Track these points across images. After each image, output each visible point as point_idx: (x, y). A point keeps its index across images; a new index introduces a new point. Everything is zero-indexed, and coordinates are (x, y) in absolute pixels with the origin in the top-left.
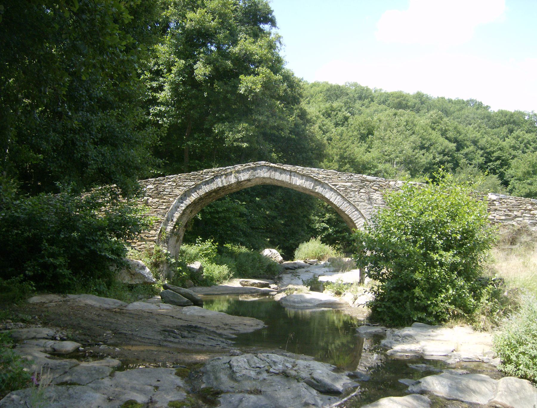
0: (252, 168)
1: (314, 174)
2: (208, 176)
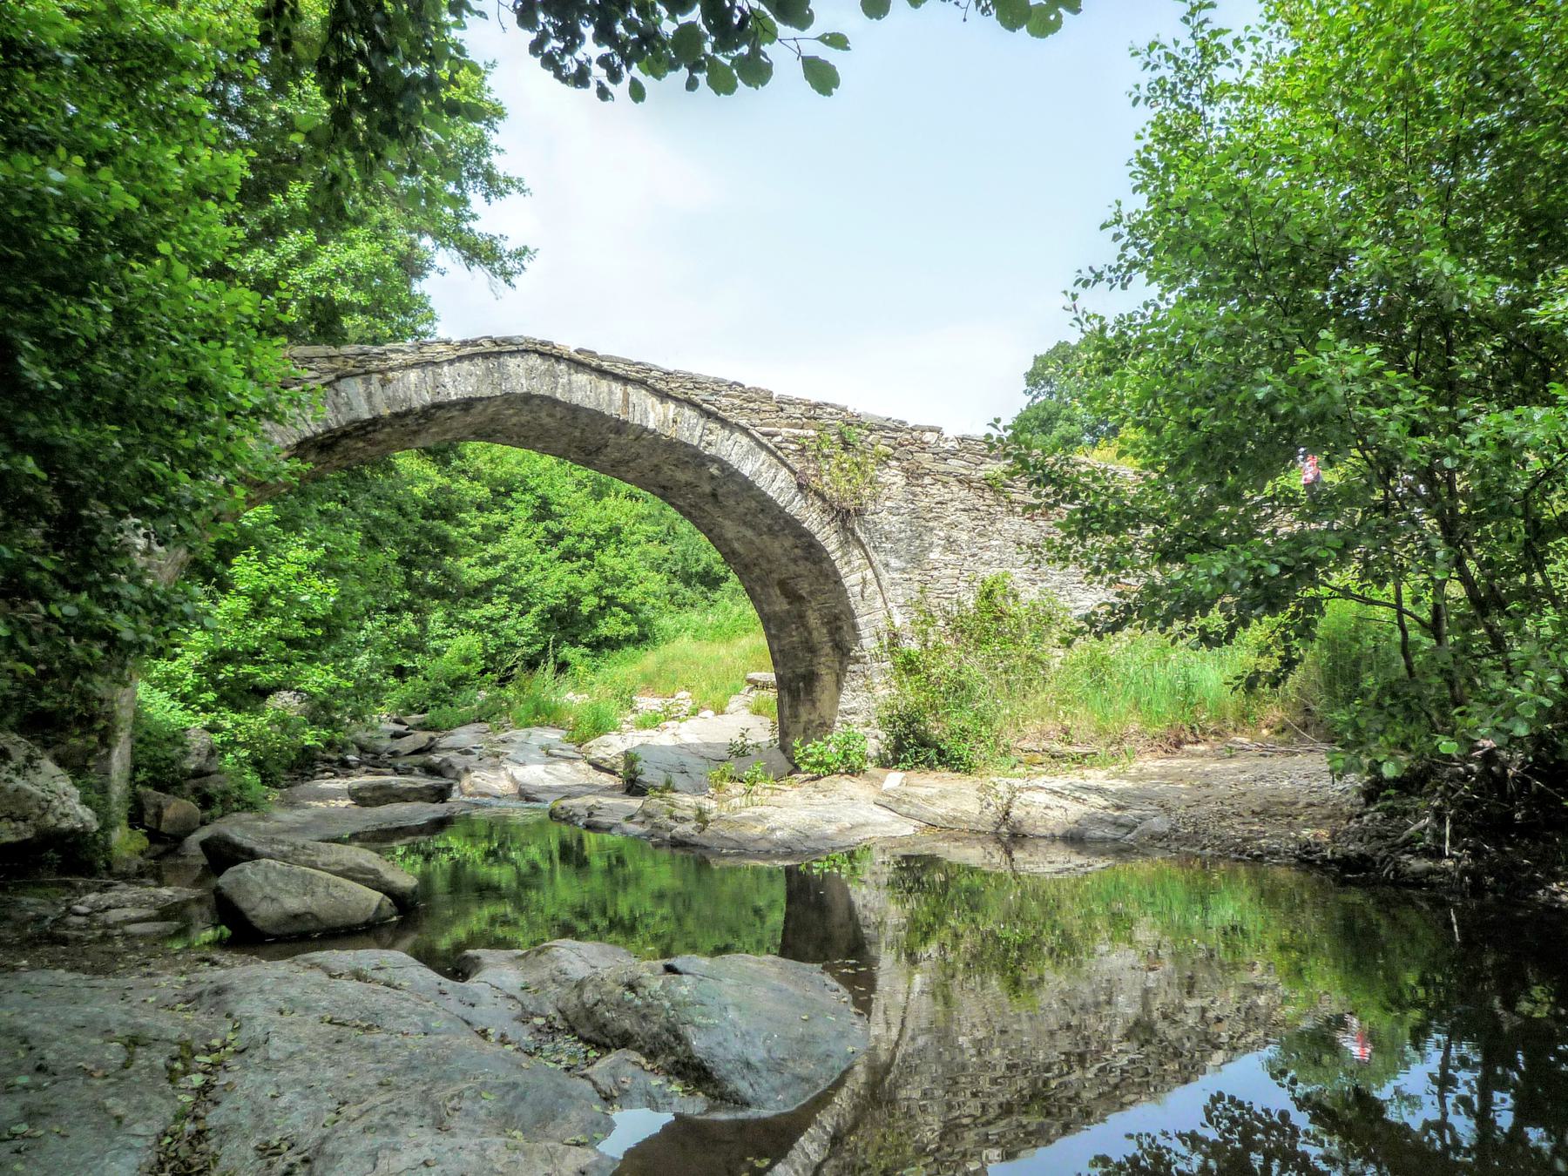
1: (704, 395)
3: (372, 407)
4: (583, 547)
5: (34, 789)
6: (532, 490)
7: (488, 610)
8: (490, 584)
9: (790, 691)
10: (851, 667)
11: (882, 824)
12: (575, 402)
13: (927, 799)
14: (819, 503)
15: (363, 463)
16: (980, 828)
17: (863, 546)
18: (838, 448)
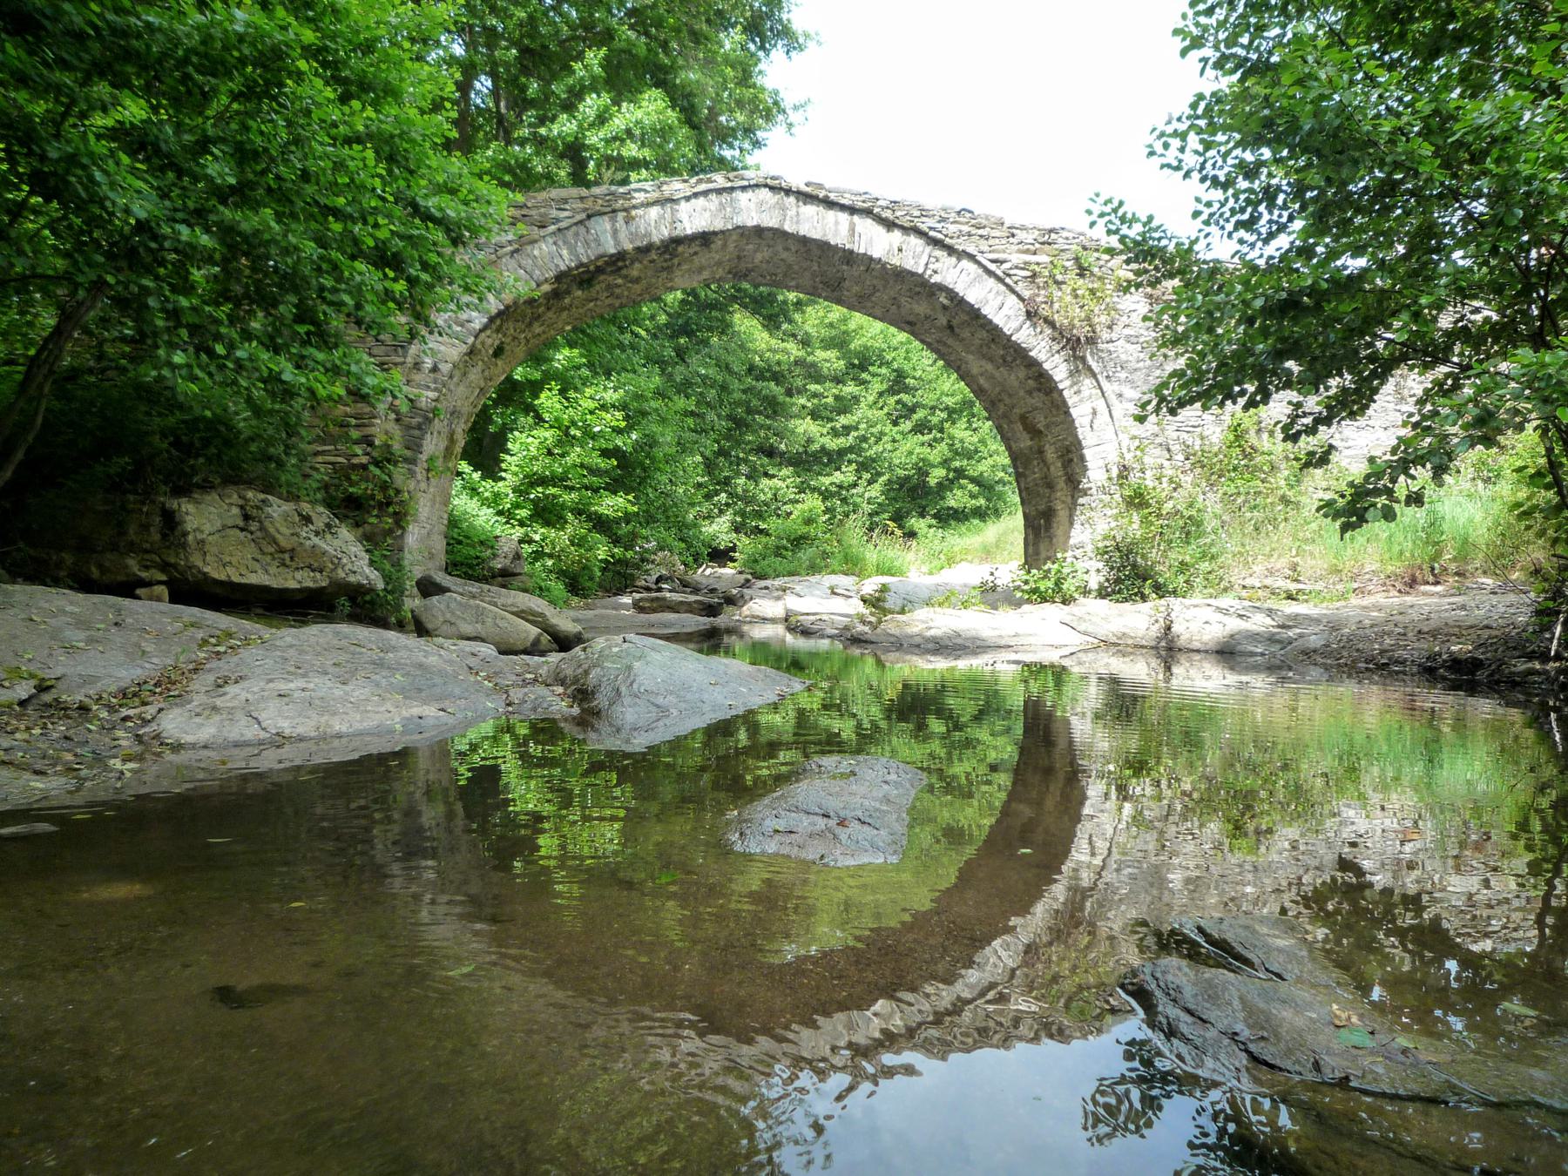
0: (719, 191)
1: (931, 222)
2: (566, 214)
3: (617, 242)
4: (935, 420)
5: (327, 548)
6: (888, 364)
7: (838, 477)
8: (842, 452)
10: (1081, 501)
12: (802, 233)
14: (1048, 331)
15: (710, 329)
17: (1094, 375)
18: (1072, 275)
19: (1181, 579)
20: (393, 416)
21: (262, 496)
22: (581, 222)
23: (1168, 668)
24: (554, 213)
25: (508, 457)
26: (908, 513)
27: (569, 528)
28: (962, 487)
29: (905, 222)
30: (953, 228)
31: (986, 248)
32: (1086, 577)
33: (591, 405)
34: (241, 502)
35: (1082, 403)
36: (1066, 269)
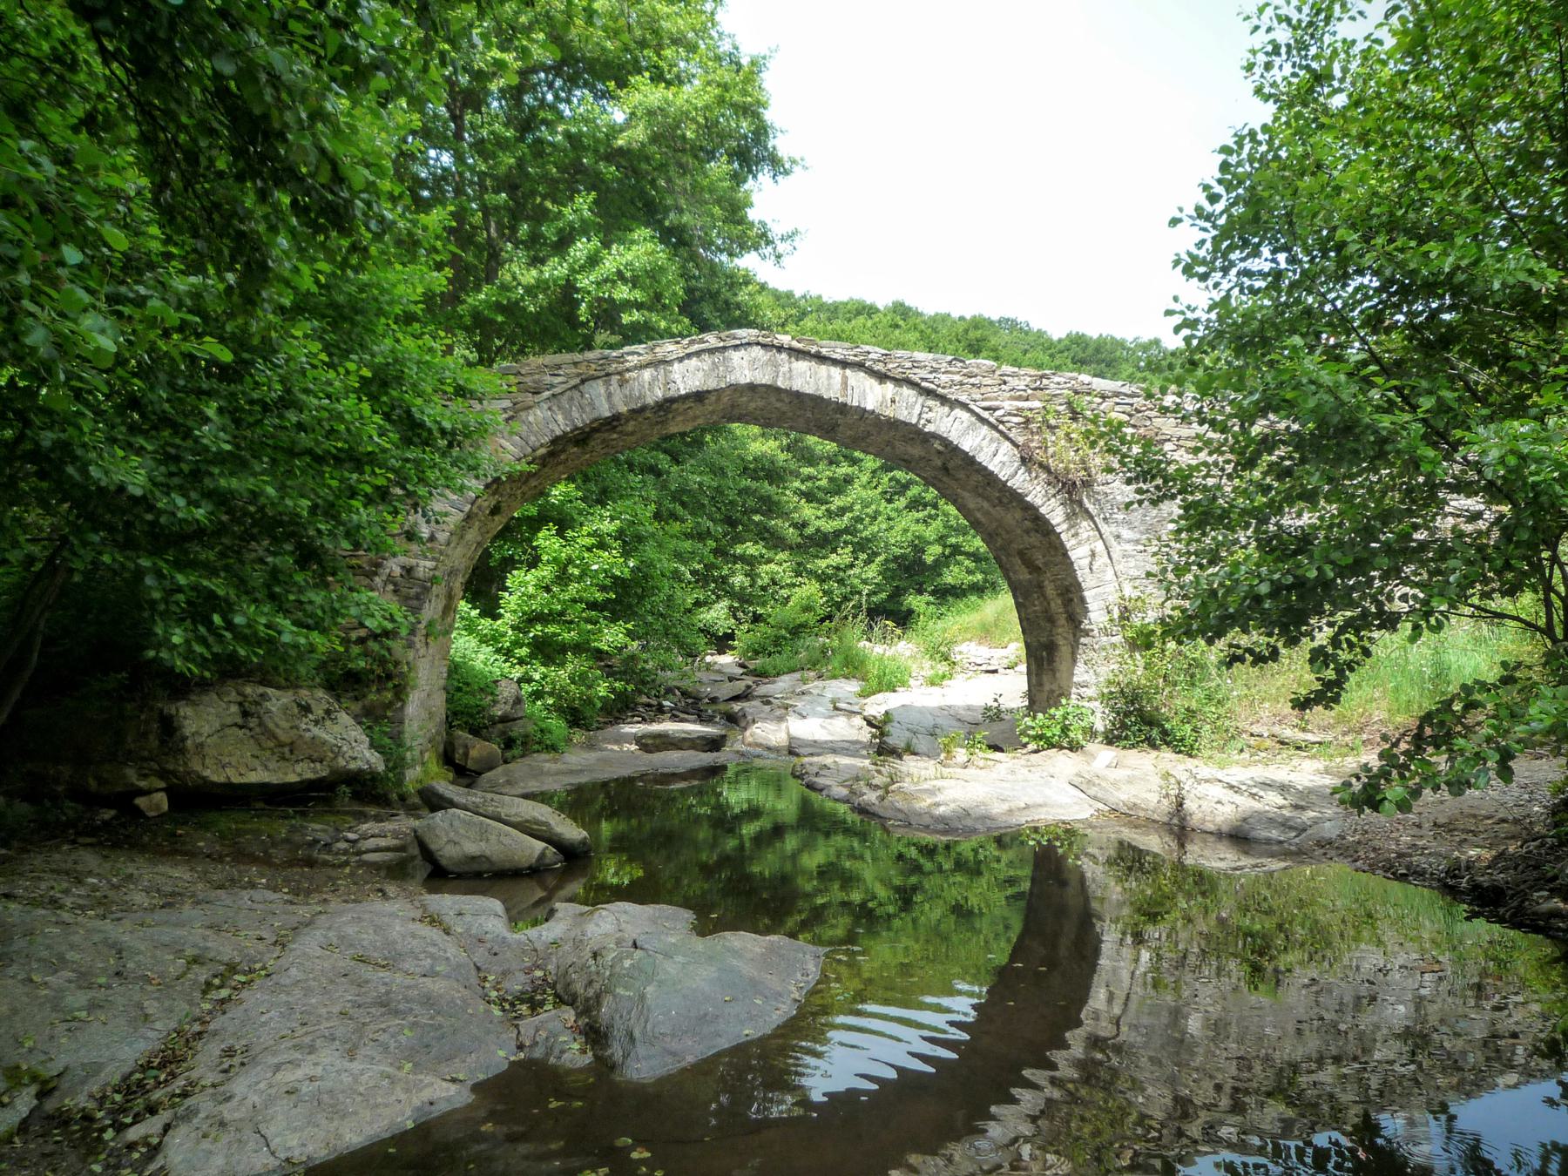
0: (711, 351)
1: (923, 373)
2: (560, 379)
3: (612, 406)
7: (834, 559)
8: (838, 534)
9: (1036, 659)
10: (1083, 640)
11: (1060, 806)
12: (795, 388)
13: (1115, 784)
16: (1156, 817)
17: (1091, 518)
18: (1065, 419)
19: (1188, 727)
20: (390, 587)
21: (261, 690)
22: (575, 387)
23: (1182, 846)
24: (548, 379)
25: (506, 594)
26: (905, 590)
27: (570, 667)
28: (958, 563)
29: (897, 373)
30: (944, 378)
31: (979, 397)
32: (1092, 719)
33: (589, 541)
34: (240, 699)
35: (1080, 547)
36: (1058, 413)
